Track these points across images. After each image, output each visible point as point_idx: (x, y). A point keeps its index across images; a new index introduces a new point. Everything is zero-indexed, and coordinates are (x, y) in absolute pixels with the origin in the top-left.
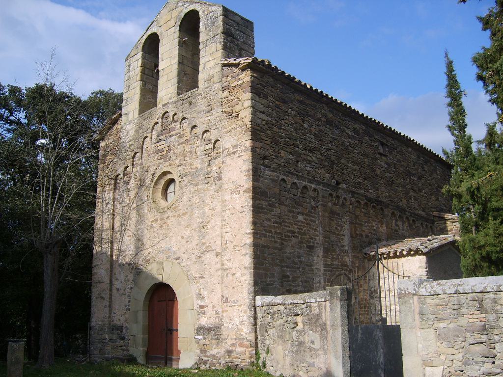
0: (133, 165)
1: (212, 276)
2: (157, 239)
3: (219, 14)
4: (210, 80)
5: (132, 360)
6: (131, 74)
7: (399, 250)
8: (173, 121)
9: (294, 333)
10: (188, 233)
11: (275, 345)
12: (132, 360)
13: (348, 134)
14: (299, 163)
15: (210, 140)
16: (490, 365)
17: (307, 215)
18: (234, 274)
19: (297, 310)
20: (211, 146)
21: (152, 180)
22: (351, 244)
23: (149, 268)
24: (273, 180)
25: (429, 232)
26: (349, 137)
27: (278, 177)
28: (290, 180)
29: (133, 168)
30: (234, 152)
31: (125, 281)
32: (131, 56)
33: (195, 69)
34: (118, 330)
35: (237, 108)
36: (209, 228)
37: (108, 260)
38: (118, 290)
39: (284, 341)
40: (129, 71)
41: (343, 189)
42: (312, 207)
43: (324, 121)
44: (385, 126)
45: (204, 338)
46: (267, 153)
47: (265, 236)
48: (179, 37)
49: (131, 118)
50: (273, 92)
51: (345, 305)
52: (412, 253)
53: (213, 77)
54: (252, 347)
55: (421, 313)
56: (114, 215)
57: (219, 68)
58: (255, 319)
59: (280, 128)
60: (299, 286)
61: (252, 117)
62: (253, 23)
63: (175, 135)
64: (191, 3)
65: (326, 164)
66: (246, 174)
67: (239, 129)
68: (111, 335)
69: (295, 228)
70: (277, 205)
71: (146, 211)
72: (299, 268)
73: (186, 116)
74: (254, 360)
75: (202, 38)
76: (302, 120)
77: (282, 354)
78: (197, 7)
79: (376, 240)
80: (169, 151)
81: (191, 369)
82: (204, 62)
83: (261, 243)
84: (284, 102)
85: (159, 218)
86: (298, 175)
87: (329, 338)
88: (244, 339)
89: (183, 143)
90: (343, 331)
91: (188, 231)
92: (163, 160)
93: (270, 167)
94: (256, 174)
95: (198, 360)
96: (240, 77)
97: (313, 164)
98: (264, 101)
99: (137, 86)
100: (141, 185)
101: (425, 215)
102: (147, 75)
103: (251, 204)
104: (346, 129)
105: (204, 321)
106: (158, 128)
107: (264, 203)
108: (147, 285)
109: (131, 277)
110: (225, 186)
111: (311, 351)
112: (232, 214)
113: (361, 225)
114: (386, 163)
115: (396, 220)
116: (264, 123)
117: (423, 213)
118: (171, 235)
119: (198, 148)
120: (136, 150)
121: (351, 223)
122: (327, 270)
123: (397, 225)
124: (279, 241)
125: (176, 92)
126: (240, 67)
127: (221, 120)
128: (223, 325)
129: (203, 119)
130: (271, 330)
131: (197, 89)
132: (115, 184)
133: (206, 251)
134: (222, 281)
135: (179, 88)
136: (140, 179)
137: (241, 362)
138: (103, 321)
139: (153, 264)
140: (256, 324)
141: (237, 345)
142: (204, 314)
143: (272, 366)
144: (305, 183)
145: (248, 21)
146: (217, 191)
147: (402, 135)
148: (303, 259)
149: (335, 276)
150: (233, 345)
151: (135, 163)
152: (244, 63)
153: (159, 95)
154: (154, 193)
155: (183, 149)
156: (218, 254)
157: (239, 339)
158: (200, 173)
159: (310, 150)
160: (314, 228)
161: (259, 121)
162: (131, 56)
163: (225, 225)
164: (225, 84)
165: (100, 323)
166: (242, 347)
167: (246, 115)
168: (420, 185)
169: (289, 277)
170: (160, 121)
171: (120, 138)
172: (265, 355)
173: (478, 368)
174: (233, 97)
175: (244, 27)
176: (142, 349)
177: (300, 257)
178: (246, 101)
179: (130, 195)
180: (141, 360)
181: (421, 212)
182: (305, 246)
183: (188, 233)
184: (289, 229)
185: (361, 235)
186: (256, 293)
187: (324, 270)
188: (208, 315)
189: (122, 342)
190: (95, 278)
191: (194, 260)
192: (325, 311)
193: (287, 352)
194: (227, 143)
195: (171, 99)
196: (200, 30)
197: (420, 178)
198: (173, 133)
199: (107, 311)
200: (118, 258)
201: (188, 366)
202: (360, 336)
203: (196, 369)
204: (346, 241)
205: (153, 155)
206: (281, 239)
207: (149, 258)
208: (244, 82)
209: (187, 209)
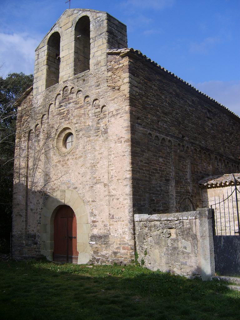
0: (42, 123)
1: (101, 200)
2: (60, 175)
3: (104, 19)
4: (98, 64)
5: (43, 259)
6: (40, 60)
7: (224, 182)
8: (71, 93)
9: (169, 241)
10: (83, 170)
11: (153, 249)
12: (43, 259)
13: (189, 103)
14: (160, 122)
15: (99, 106)
17: (165, 158)
18: (118, 199)
19: (170, 225)
20: (99, 110)
21: (56, 134)
22: (191, 178)
23: (55, 194)
24: (144, 134)
25: (236, 170)
26: (190, 106)
27: (146, 131)
28: (155, 134)
29: (42, 125)
30: (117, 114)
31: (37, 204)
32: (39, 48)
33: (85, 57)
34: (32, 237)
35: (119, 83)
36: (98, 167)
37: (24, 189)
38: (32, 210)
39: (160, 247)
40: (38, 59)
41: (186, 141)
42: (168, 152)
43: (174, 95)
44: (211, 99)
45: (96, 244)
46: (140, 115)
47: (139, 172)
48: (75, 35)
49: (40, 91)
50: (142, 73)
51: (211, 221)
52: (233, 183)
53: (100, 62)
54: (132, 249)
56: (28, 158)
57: (104, 56)
58: (134, 230)
59: (147, 98)
60: (160, 207)
61: (130, 90)
62: (126, 26)
63: (73, 103)
64: (83, 11)
65: (176, 123)
66: (126, 129)
68: (27, 241)
69: (157, 167)
70: (146, 151)
72: (160, 194)
73: (81, 89)
74: (133, 258)
75: (92, 35)
76: (161, 93)
77: (158, 255)
78: (88, 14)
79: (206, 175)
80: (68, 114)
81: (87, 264)
82: (94, 52)
83: (137, 177)
84: (150, 80)
85: (61, 159)
86: (159, 131)
87: (199, 245)
88: (126, 244)
89: (78, 108)
90: (210, 239)
92: (64, 120)
93: (141, 125)
94: (133, 129)
95: (92, 258)
96: (120, 62)
97: (168, 123)
98: (137, 79)
99: (44, 69)
100: (48, 137)
101: (234, 159)
102: (51, 61)
103: (129, 150)
104: (188, 101)
105: (95, 232)
106: (60, 97)
107: (139, 150)
108: (54, 206)
109: (41, 201)
110: (110, 138)
111: (183, 254)
112: (116, 157)
113: (197, 165)
114: (211, 124)
115: (218, 162)
116: (137, 94)
117: (233, 158)
118: (70, 171)
119: (90, 112)
120: (44, 113)
121: (192, 163)
122: (177, 195)
123: (218, 165)
124: (148, 176)
125: (73, 72)
126: (121, 55)
127: (107, 92)
128: (110, 234)
129: (94, 91)
130: (149, 238)
131: (88, 70)
132: (29, 136)
134: (109, 203)
135: (75, 70)
136: (47, 133)
139: (57, 192)
140: (134, 234)
141: (121, 248)
142: (96, 226)
143: (150, 264)
144: (163, 136)
145: (123, 25)
146: (104, 141)
147: (221, 105)
149: (182, 200)
150: (118, 248)
151: (43, 122)
152: (124, 52)
153: (61, 75)
154: (57, 142)
156: (105, 185)
157: (122, 244)
158: (92, 128)
159: (166, 114)
160: (169, 167)
161: (134, 92)
162: (39, 48)
163: (110, 165)
164: (109, 67)
165: (19, 233)
166: (124, 249)
167: (126, 88)
168: (231, 139)
169: (154, 201)
170: (61, 92)
171: (32, 105)
172: (143, 255)
174: (115, 76)
175: (121, 28)
176: (50, 251)
177: (161, 187)
178: (125, 79)
179: (40, 144)
180: (49, 258)
181: (231, 157)
182: (164, 179)
183: (83, 170)
184: (154, 167)
185: (198, 172)
186: (135, 212)
187: (176, 195)
188: (99, 227)
189: (35, 246)
190: (15, 202)
191: (88, 189)
192: (196, 226)
193: (163, 254)
194: (111, 107)
195: (69, 77)
196: (91, 30)
197: (231, 134)
198: (71, 101)
199: (24, 225)
200: (32, 188)
201: (85, 263)
202: (222, 243)
203: (91, 265)
204: (188, 176)
205: (57, 116)
206: (149, 174)
207: (54, 187)
208: (123, 65)
209: (82, 153)
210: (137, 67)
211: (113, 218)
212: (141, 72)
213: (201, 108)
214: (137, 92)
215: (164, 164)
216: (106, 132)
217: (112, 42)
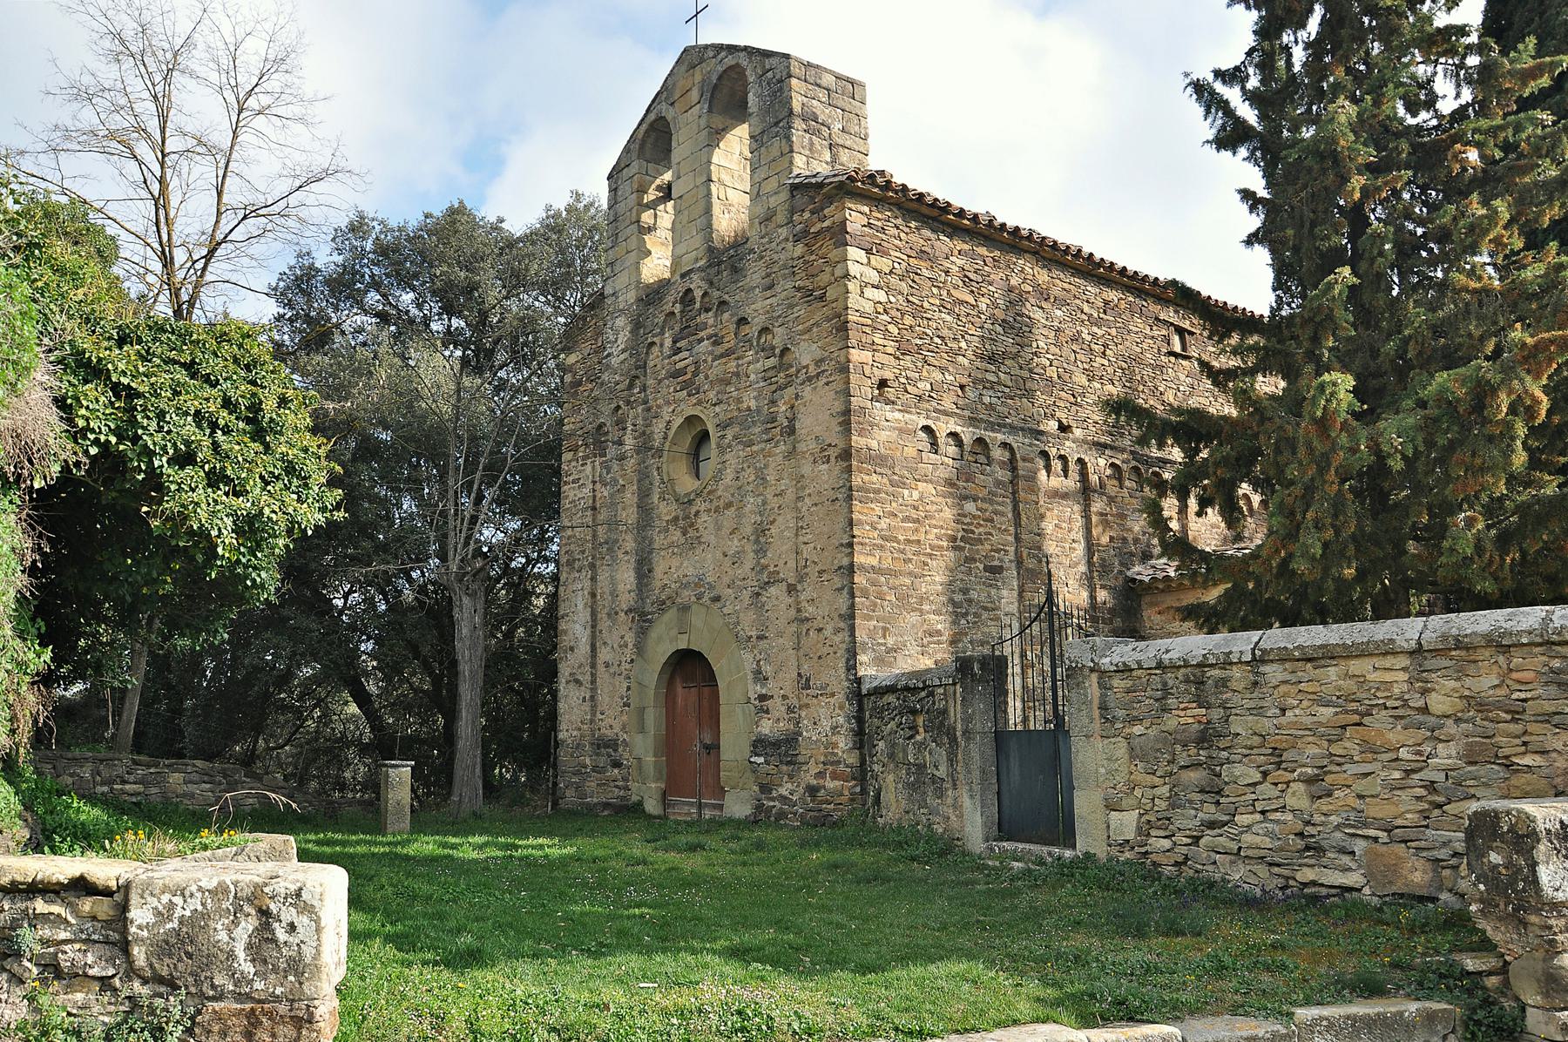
16: (1212, 809)
18: (820, 630)
34: (605, 744)
38: (607, 665)
40: (616, 203)
45: (767, 762)
55: (1103, 707)
67: (826, 325)
71: (656, 500)
88: (839, 762)
89: (722, 356)
91: (736, 542)
92: (685, 392)
97: (1002, 388)
105: (766, 727)
110: (801, 447)
127: (791, 306)
128: (801, 735)
129: (758, 305)
133: (768, 583)
137: (834, 810)
138: (580, 729)
142: (767, 712)
148: (974, 595)
150: (820, 775)
155: (722, 368)
156: (791, 589)
165: (575, 733)
170: (677, 308)
173: (1193, 812)
174: (813, 257)
183: (734, 545)
189: (616, 771)
190: (565, 641)
191: (747, 601)
195: (697, 260)
198: (702, 334)
216: (791, 430)
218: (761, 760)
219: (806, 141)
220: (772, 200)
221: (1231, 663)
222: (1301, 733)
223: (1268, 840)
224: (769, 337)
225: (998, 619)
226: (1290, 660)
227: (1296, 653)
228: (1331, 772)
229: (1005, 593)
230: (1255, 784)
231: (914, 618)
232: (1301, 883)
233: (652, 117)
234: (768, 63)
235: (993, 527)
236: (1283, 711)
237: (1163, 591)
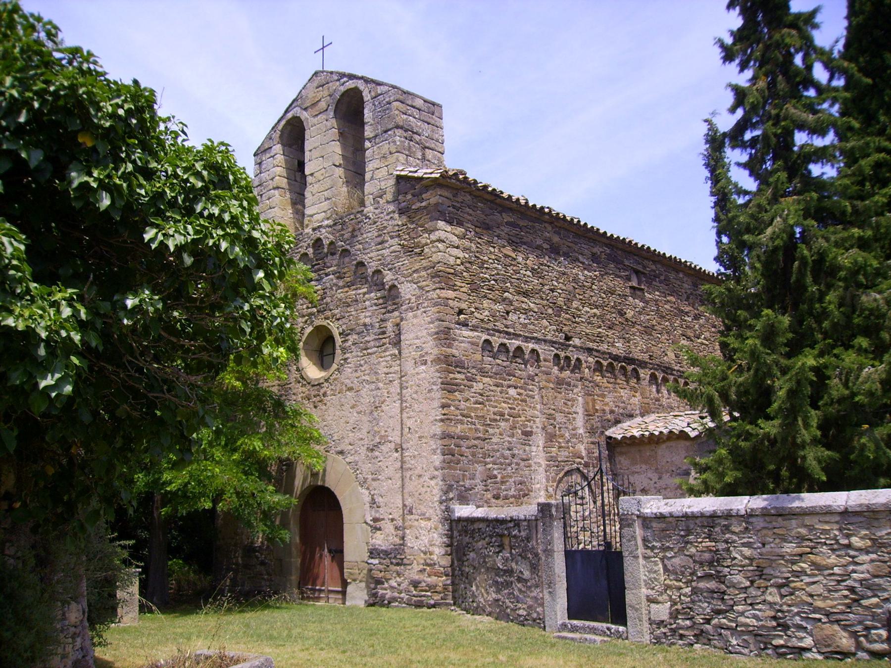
18: (420, 476)
24: (473, 344)
28: (496, 341)
46: (464, 306)
70: (478, 377)
93: (467, 325)
96: (424, 196)
104: (580, 257)
110: (405, 352)
113: (603, 396)
116: (459, 262)
124: (481, 427)
127: (397, 257)
142: (380, 529)
150: (422, 571)
164: (403, 204)
182: (520, 432)
208: (429, 204)
210: (458, 205)
211: (411, 513)
212: (468, 214)
213: (615, 269)
214: (459, 258)
215: (521, 401)
216: (397, 343)
217: (410, 147)
218: (376, 561)
219: (406, 144)
220: (383, 183)
221: (732, 516)
222: (774, 558)
223: (754, 621)
224: (380, 277)
225: (530, 466)
226: (768, 515)
227: (772, 511)
228: (793, 581)
229: (534, 449)
230: (746, 588)
231: (480, 468)
232: (774, 646)
233: (289, 115)
234: (380, 89)
235: (527, 405)
236: (764, 545)
237: (629, 445)
